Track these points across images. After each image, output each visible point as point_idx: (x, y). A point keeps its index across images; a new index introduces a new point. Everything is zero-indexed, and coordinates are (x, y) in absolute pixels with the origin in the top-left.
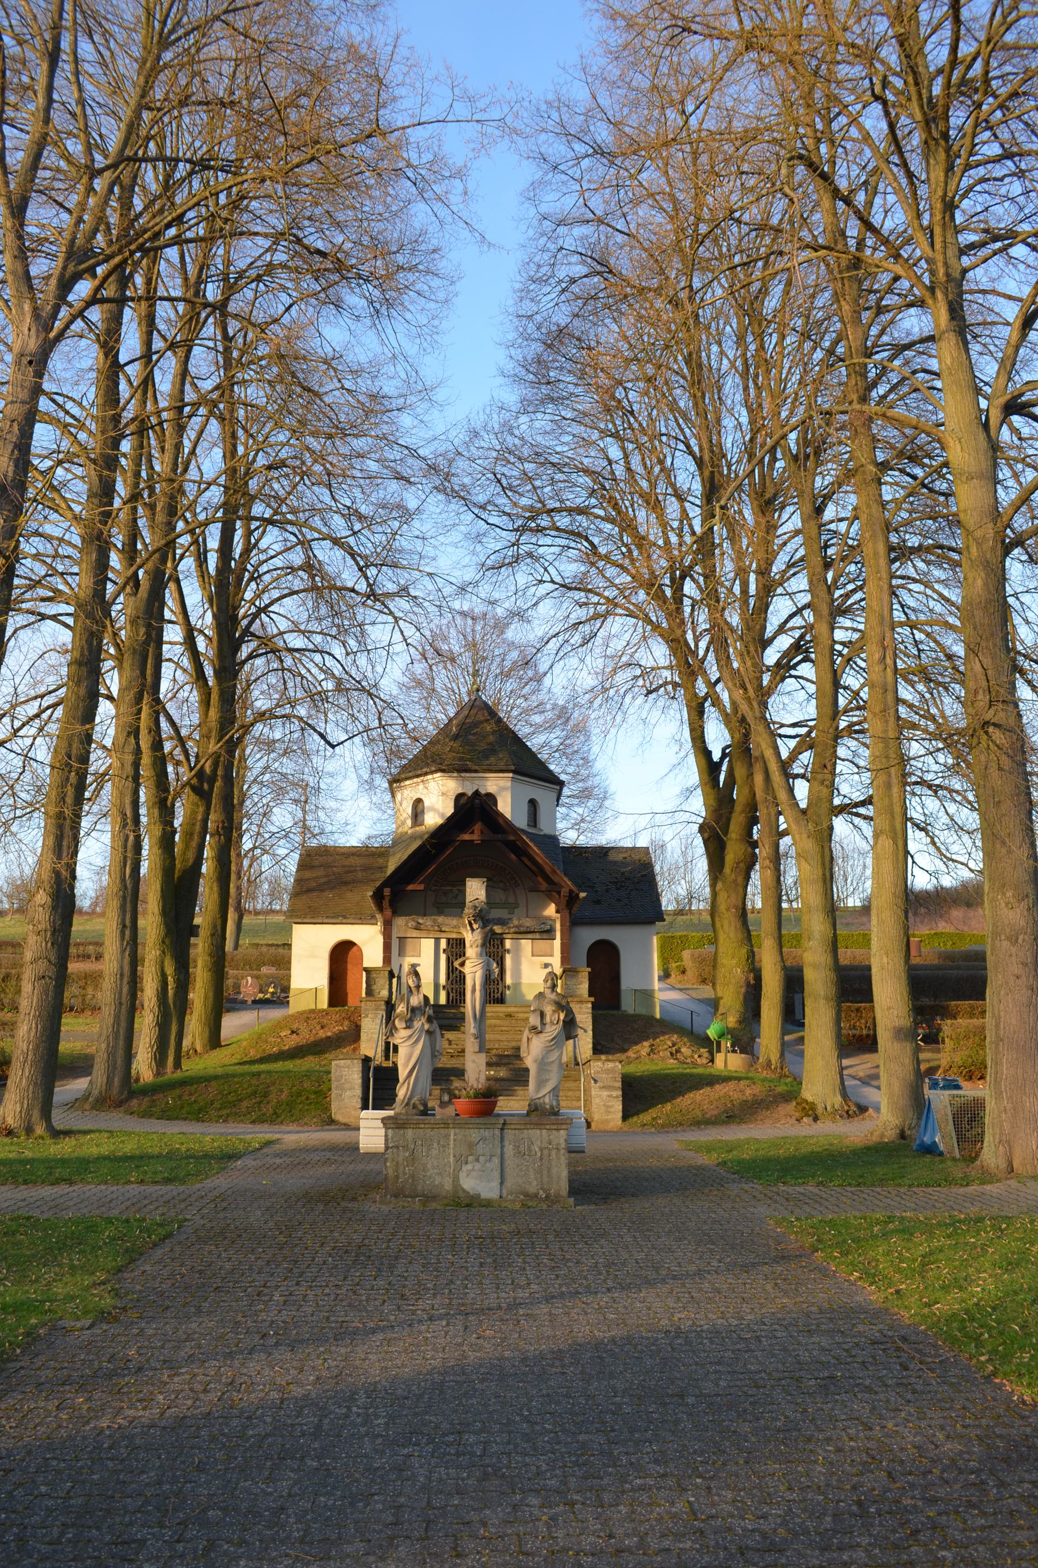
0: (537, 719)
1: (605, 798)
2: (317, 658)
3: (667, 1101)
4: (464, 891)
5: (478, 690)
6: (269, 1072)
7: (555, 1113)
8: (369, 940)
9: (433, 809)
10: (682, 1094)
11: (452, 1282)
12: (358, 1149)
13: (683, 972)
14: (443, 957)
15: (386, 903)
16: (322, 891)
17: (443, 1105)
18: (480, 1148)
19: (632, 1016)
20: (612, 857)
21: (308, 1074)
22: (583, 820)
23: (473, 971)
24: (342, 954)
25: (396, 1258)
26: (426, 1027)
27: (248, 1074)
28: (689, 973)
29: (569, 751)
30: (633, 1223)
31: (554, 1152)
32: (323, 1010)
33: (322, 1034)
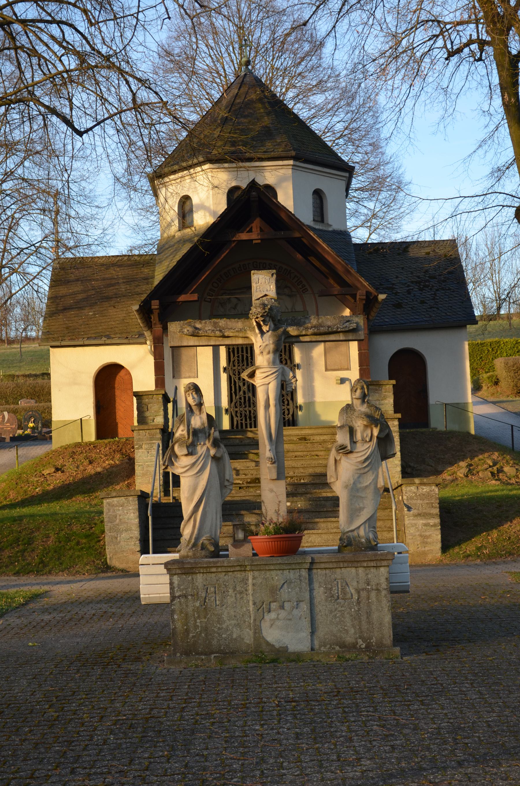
0: (318, 99)
1: (399, 189)
2: (54, 30)
3: (492, 528)
4: (250, 288)
5: (248, 63)
6: (32, 516)
7: (371, 547)
8: (138, 362)
9: (202, 207)
10: (509, 519)
11: (263, 760)
12: (138, 598)
13: (496, 383)
14: (224, 377)
15: (155, 318)
16: (81, 308)
17: (237, 543)
18: (284, 593)
19: (445, 433)
20: (413, 253)
21: (77, 516)
22: (374, 216)
23: (265, 382)
24: (108, 379)
25: (193, 732)
26: (212, 452)
27: (8, 519)
28: (503, 384)
29: (355, 136)
30: (475, 675)
31: (373, 594)
32: (90, 443)
33: (91, 470)
